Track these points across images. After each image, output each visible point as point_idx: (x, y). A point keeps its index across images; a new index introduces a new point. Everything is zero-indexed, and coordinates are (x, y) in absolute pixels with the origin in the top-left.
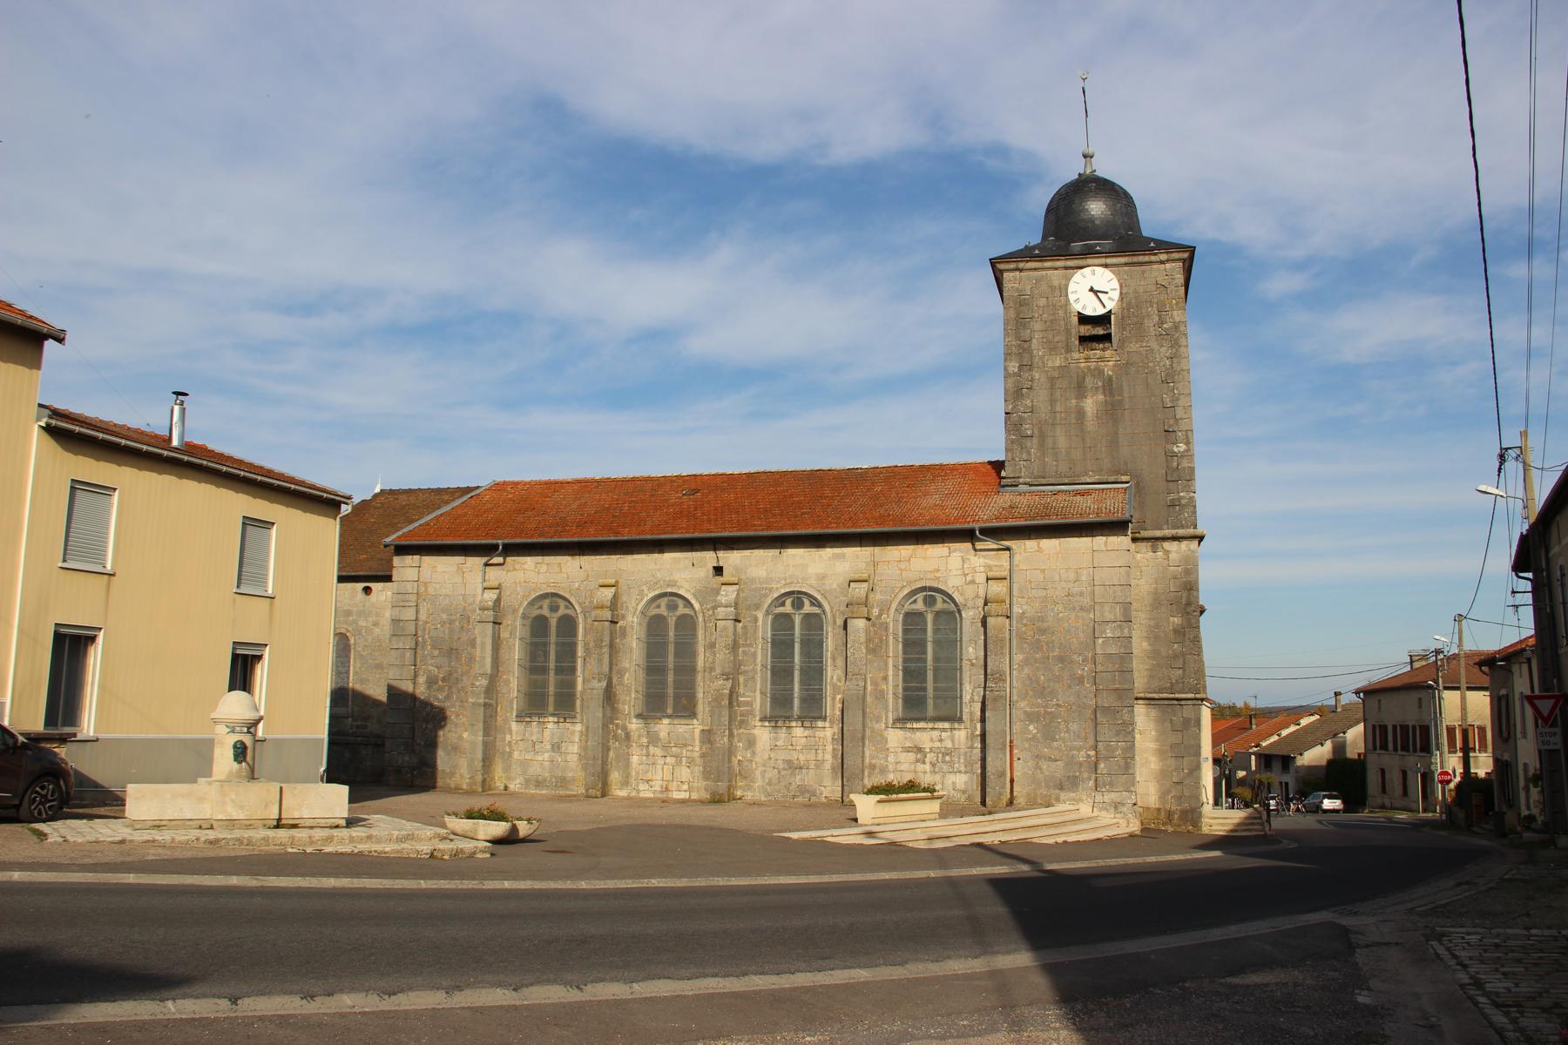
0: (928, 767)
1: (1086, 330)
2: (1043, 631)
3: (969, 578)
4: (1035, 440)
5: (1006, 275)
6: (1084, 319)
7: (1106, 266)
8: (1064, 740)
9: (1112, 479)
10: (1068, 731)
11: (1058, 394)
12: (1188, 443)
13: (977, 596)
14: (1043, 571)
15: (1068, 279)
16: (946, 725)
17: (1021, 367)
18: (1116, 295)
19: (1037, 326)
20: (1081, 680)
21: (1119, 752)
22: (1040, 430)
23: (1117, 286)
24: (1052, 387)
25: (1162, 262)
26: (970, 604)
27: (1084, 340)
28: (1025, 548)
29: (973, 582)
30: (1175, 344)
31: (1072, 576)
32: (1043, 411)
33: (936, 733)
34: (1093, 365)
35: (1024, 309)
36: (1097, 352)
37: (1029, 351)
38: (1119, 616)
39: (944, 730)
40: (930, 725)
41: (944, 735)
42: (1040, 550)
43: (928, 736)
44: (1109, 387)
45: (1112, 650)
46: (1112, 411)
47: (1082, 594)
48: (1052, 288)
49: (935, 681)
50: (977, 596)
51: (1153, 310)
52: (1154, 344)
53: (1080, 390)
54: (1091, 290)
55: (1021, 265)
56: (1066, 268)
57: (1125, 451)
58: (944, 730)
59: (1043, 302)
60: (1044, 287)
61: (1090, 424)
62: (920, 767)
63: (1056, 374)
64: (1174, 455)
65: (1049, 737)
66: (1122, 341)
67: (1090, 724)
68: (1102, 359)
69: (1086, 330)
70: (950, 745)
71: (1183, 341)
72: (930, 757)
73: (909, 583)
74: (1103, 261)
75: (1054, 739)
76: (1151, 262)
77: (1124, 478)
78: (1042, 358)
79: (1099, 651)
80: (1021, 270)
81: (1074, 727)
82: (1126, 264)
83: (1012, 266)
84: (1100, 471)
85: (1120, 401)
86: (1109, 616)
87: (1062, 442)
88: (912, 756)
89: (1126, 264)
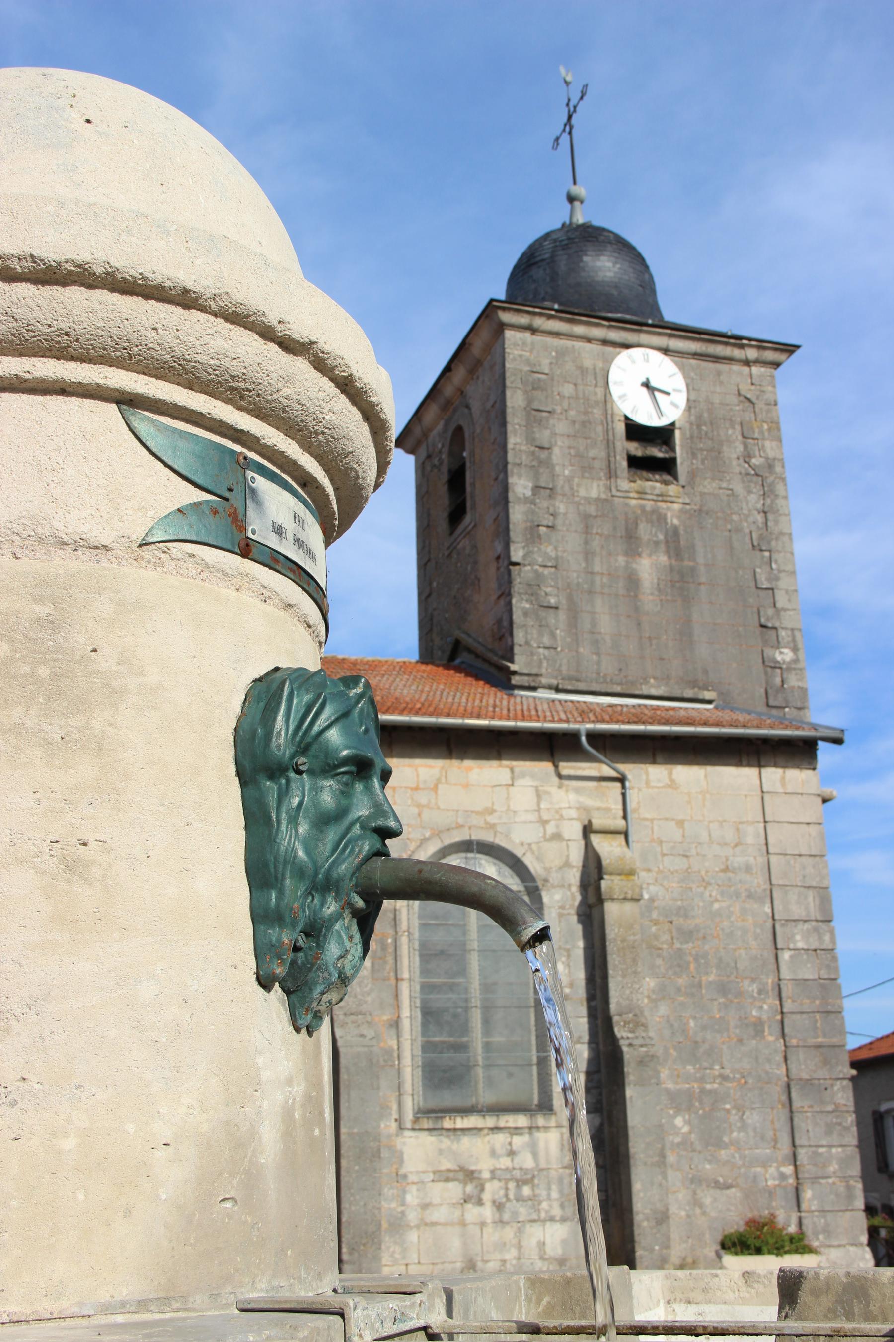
0: (488, 1212)
1: (635, 449)
2: (688, 935)
3: (551, 829)
4: (562, 615)
5: (508, 334)
6: (635, 431)
7: (666, 351)
8: (735, 1143)
9: (689, 694)
10: (744, 1127)
11: (596, 543)
12: (795, 649)
13: (567, 864)
14: (680, 823)
15: (608, 361)
16: (521, 1120)
17: (537, 488)
18: (681, 399)
19: (561, 427)
20: (758, 1028)
21: (833, 1167)
22: (570, 599)
23: (683, 387)
24: (587, 530)
25: (747, 363)
26: (554, 878)
27: (635, 463)
28: (649, 778)
29: (557, 837)
30: (768, 492)
31: (729, 835)
32: (574, 566)
33: (500, 1139)
34: (649, 505)
35: (538, 394)
36: (654, 484)
37: (548, 464)
38: (815, 913)
39: (517, 1131)
40: (490, 1122)
41: (518, 1141)
42: (673, 785)
43: (483, 1147)
44: (674, 544)
45: (808, 972)
46: (681, 582)
47: (748, 869)
48: (583, 371)
49: (487, 1032)
50: (567, 864)
51: (735, 434)
52: (739, 488)
53: (631, 542)
54: (646, 385)
55: (539, 322)
56: (605, 342)
57: (703, 651)
58: (517, 1131)
59: (568, 389)
60: (569, 366)
61: (648, 599)
62: (472, 1212)
63: (592, 510)
64: (777, 665)
65: (712, 1139)
66: (693, 475)
67: (782, 1114)
68: (662, 497)
69: (635, 449)
70: (528, 1162)
71: (780, 488)
72: (492, 1190)
73: (438, 833)
74: (663, 341)
75: (719, 1144)
76: (730, 360)
77: (708, 695)
78: (569, 480)
79: (785, 973)
80: (533, 330)
81: (753, 1118)
82: (696, 355)
83: (524, 320)
84: (666, 679)
85: (693, 570)
86: (797, 911)
87: (606, 625)
88: (455, 1190)
89: (696, 355)
